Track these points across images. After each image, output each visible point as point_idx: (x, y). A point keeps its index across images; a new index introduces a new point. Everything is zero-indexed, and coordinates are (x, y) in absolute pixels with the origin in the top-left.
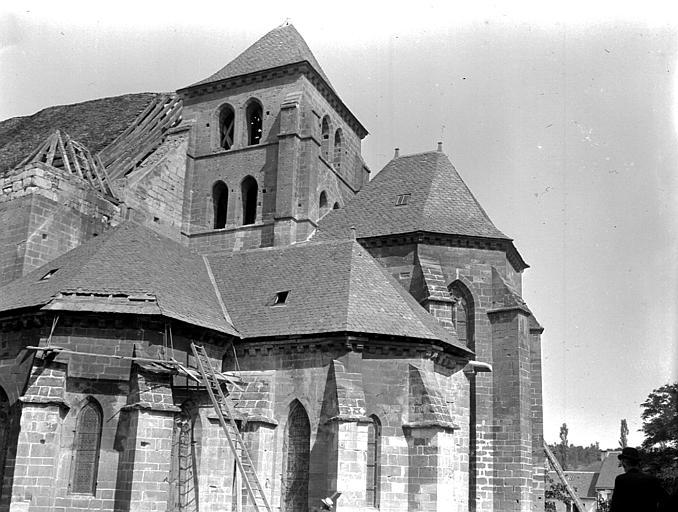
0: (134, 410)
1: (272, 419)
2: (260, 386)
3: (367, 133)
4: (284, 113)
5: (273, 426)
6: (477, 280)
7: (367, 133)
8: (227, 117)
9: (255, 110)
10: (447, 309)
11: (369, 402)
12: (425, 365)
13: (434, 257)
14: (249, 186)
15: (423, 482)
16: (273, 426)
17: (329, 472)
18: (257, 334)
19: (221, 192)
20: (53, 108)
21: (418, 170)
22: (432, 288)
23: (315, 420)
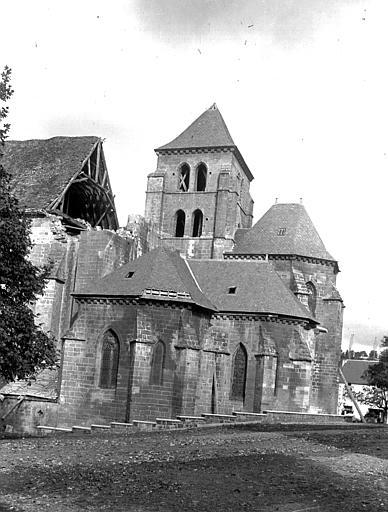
0: (135, 342)
1: (228, 351)
2: (223, 335)
3: (212, 118)
4: (221, 177)
5: (228, 354)
6: (319, 282)
7: (212, 118)
8: (185, 169)
9: (202, 170)
10: (306, 298)
11: (276, 347)
12: (300, 328)
13: (299, 269)
14: (198, 215)
15: (297, 385)
16: (228, 354)
17: (102, 374)
18: (223, 310)
19: (181, 215)
20: (61, 138)
21: (288, 214)
22: (300, 286)
23: (251, 355)
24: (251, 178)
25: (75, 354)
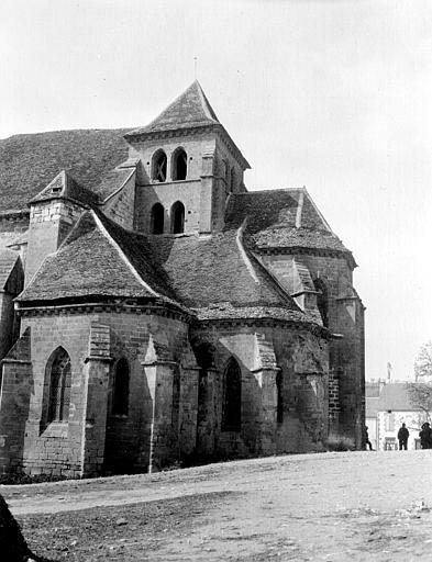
9: (181, 157)
24: (245, 165)
25: (17, 382)
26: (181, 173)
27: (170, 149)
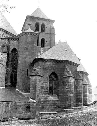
9: (43, 26)
26: (43, 31)
27: (41, 23)
